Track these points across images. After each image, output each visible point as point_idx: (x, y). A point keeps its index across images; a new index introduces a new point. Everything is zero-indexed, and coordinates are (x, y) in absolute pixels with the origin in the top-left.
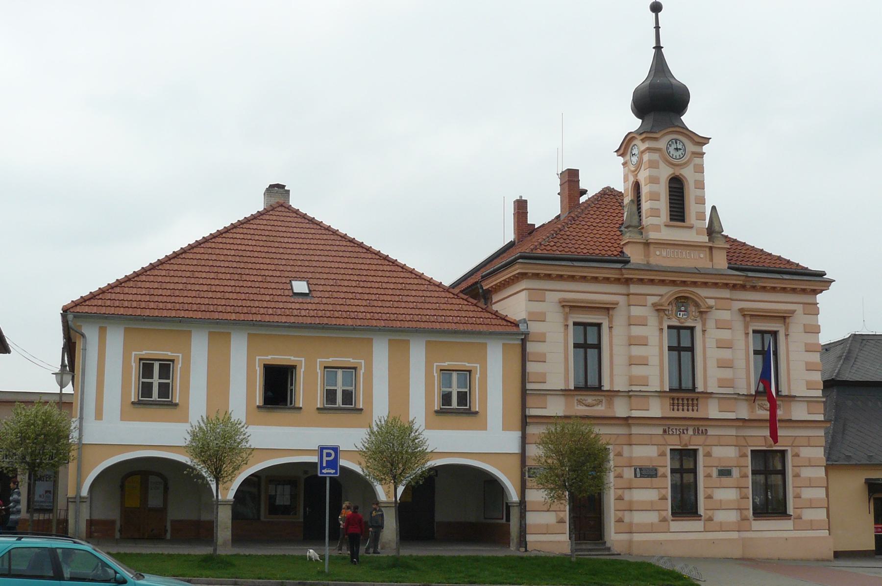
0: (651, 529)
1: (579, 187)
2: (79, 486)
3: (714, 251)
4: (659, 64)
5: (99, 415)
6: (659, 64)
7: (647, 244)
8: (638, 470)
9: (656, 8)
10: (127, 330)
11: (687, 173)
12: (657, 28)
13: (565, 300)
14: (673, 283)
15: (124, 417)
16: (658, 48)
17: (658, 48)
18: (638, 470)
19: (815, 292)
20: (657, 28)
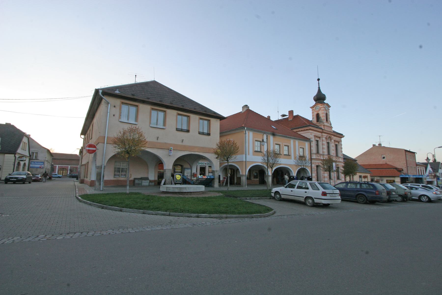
0: (253, 173)
1: (266, 118)
2: (246, 173)
3: (103, 144)
4: (319, 91)
5: (249, 154)
6: (319, 91)
7: (324, 126)
8: (95, 149)
9: (319, 80)
10: (253, 133)
11: (328, 112)
12: (319, 84)
13: (315, 135)
14: (328, 134)
15: (254, 155)
16: (319, 88)
17: (319, 88)
18: (95, 149)
19: (341, 138)
20: (319, 84)
